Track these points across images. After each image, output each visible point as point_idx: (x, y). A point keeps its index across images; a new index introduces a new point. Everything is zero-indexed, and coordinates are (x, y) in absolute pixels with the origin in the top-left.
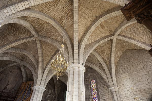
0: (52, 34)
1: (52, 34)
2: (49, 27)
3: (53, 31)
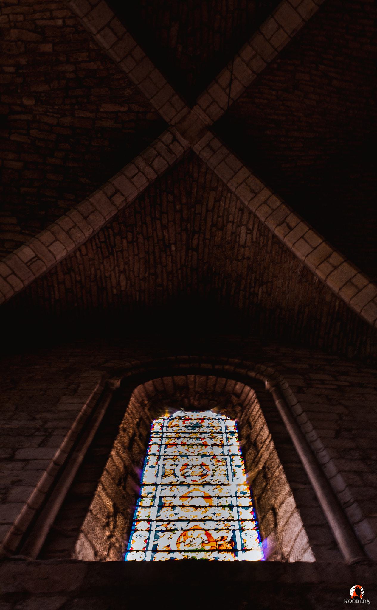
0: (47, 48)
1: (47, 48)
2: (27, 102)
3: (23, 61)
